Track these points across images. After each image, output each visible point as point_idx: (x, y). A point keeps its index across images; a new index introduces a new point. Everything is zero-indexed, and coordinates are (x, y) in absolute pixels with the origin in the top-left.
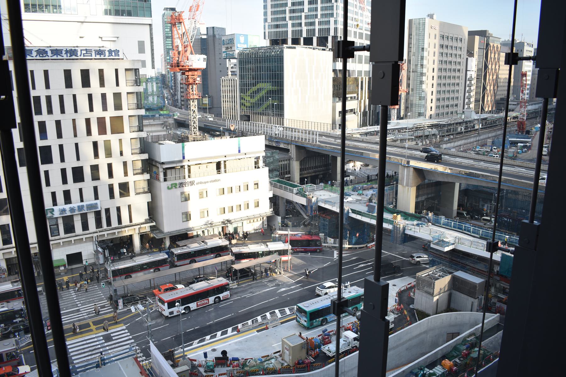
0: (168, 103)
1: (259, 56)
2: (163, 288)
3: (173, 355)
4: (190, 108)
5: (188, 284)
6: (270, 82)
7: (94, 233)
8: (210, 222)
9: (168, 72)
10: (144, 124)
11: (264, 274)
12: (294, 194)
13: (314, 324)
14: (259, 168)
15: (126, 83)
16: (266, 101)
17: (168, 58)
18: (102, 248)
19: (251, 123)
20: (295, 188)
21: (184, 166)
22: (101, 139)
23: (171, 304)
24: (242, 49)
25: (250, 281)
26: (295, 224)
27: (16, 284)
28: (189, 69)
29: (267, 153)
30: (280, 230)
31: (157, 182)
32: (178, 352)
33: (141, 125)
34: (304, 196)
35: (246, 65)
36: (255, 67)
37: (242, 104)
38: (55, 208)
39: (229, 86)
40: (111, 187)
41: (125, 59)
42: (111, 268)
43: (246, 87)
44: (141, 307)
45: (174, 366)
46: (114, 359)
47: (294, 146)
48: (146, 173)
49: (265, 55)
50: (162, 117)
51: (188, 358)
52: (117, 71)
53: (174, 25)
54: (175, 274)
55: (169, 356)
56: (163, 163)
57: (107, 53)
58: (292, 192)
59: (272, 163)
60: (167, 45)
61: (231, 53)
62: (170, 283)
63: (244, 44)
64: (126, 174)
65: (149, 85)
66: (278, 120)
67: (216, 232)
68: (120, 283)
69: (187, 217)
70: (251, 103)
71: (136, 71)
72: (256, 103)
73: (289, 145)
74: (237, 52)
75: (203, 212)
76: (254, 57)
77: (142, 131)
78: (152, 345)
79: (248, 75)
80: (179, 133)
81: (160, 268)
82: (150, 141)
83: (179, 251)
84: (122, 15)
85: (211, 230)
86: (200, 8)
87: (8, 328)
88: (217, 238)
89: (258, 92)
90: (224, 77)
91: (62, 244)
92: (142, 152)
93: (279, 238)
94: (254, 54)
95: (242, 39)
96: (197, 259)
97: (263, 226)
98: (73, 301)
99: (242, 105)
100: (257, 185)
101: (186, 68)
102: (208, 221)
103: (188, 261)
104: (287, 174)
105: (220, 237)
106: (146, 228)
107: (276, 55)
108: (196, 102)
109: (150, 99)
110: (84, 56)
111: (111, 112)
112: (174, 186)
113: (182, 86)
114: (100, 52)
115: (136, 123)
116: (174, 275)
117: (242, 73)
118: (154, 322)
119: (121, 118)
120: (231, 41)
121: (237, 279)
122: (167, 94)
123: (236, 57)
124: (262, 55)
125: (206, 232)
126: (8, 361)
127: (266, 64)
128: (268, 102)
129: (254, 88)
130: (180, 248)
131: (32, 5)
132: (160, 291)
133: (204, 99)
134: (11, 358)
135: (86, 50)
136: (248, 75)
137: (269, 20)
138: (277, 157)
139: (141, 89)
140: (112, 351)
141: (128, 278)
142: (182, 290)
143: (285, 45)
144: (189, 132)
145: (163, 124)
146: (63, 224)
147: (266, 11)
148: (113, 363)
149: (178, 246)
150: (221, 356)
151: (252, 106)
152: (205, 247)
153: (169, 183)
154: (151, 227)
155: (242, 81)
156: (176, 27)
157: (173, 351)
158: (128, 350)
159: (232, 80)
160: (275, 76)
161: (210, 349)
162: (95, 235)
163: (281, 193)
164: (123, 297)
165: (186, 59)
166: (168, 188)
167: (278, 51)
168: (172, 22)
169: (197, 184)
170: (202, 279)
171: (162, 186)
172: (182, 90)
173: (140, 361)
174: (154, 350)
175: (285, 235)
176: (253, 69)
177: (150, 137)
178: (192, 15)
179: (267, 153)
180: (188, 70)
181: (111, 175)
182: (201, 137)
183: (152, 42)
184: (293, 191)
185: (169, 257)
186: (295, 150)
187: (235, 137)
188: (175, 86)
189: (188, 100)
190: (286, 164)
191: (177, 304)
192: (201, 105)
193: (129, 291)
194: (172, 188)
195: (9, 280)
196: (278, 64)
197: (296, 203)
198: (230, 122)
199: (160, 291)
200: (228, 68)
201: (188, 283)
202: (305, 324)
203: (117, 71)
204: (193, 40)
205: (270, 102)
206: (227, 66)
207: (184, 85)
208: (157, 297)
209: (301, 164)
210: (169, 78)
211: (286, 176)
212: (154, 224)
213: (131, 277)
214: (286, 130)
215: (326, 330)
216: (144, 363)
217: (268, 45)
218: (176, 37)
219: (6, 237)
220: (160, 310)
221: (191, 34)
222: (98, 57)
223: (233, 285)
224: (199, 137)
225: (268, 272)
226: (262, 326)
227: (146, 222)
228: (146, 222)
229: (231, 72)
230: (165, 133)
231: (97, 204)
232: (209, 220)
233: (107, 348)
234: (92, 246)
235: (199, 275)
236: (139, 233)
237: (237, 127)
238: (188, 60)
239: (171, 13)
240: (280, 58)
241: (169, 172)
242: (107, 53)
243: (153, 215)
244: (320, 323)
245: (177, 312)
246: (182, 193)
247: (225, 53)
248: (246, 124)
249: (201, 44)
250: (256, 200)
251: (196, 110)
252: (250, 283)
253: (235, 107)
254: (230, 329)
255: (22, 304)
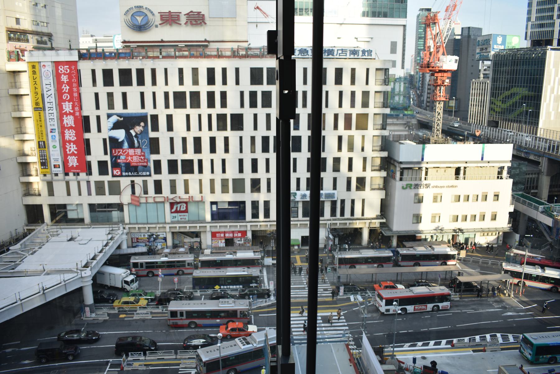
0: (414, 104)
1: (517, 58)
2: (384, 284)
3: (383, 352)
4: (435, 109)
5: (409, 285)
6: (527, 87)
7: (328, 220)
8: (440, 228)
9: (417, 73)
10: (387, 123)
11: (491, 292)
12: (539, 213)
13: (541, 360)
14: (503, 179)
15: (376, 82)
16: (519, 107)
17: (419, 58)
18: (333, 235)
19: (499, 130)
20: (541, 206)
21: (422, 168)
22: (346, 134)
23: (389, 302)
24: (498, 50)
25: (474, 297)
26: (535, 245)
27: (257, 254)
28: (439, 70)
29: (514, 164)
30: (516, 248)
31: (393, 181)
32: (388, 350)
33: (385, 123)
34: (551, 216)
35: (501, 68)
36: (511, 70)
37: (491, 109)
38: (298, 192)
39: (480, 89)
40: (349, 180)
41: (377, 59)
42: (339, 255)
43: (499, 90)
44: (360, 298)
45: (382, 362)
46: (327, 340)
47: (547, 159)
48: (383, 170)
49: (524, 57)
50: (405, 117)
51: (397, 359)
52: (368, 70)
53: (427, 25)
54: (397, 273)
55: (379, 352)
56: (401, 163)
57: (361, 53)
58: (537, 209)
59: (518, 174)
60: (419, 45)
61: (485, 54)
62: (391, 281)
63: (501, 45)
64: (364, 169)
65: (397, 85)
66: (530, 129)
67: (445, 239)
68: (345, 272)
69: (417, 220)
70: (502, 108)
71: (386, 70)
72: (507, 109)
73: (541, 158)
74: (492, 53)
75: (435, 217)
76: (511, 58)
77: (385, 129)
78: (364, 337)
79: (502, 78)
80: (420, 134)
81: (384, 265)
82: (391, 139)
83: (405, 252)
84: (378, 17)
85: (440, 236)
86: (457, 7)
87: (245, 290)
88: (446, 246)
89: (511, 97)
90: (475, 80)
91: (299, 225)
92: (382, 149)
93: (514, 258)
94: (511, 56)
95: (499, 40)
96: (421, 263)
97: (498, 241)
98: (300, 279)
99: (492, 110)
100: (497, 197)
101: (436, 69)
102: (439, 227)
103: (412, 263)
104: (533, 189)
105: (449, 245)
106: (376, 224)
107: (537, 58)
108: (442, 105)
109: (397, 98)
110: (340, 55)
111: (358, 109)
112: (409, 186)
113: (429, 87)
114: (354, 52)
115: (380, 121)
116: (396, 274)
117: (495, 75)
118: (369, 315)
119: (366, 115)
120: (487, 42)
121: (460, 291)
122: (413, 95)
123: (491, 59)
124: (521, 57)
125: (435, 238)
126: (240, 318)
127: (527, 67)
128: (522, 109)
129: (507, 93)
130: (406, 249)
131: (300, 9)
132: (380, 286)
133: (451, 102)
134: (244, 316)
135: (342, 50)
136: (502, 78)
137: (533, 19)
138: (524, 169)
139: (388, 88)
140: (327, 332)
141: (352, 268)
142: (401, 291)
143: (549, 47)
144: (431, 134)
145: (405, 124)
146: (303, 208)
147: (530, 9)
148: (326, 344)
149: (404, 246)
150: (430, 366)
151: (503, 112)
152: (432, 252)
153: (404, 183)
154: (381, 223)
155: (494, 85)
156: (430, 27)
157: (383, 348)
158: (341, 336)
159: (483, 83)
160: (533, 80)
161: (420, 356)
162: (329, 222)
163: (523, 208)
164: (345, 285)
165: (437, 60)
166: (403, 188)
167: (540, 53)
168: (426, 22)
169: (433, 187)
170: (424, 284)
171: (398, 185)
172: (429, 91)
173: (351, 349)
174: (365, 341)
175: (521, 255)
176: (508, 72)
177: (391, 136)
178: (448, 15)
179: (514, 164)
180: (438, 71)
181: (350, 168)
182: (443, 140)
183: (404, 43)
184: (538, 209)
185: (394, 255)
186: (546, 163)
187: (479, 143)
188: (422, 87)
189: (434, 102)
190: (534, 178)
191: (394, 303)
192: (447, 107)
193: (351, 281)
194: (406, 188)
195: (252, 249)
196: (538, 67)
197: (540, 222)
198: (475, 127)
199: (380, 286)
200: (480, 70)
201: (409, 285)
202: (529, 357)
203: (368, 70)
204: (446, 41)
205: (523, 108)
206: (480, 68)
207: (432, 86)
208: (376, 292)
209: (552, 180)
210: (417, 78)
211: (532, 191)
212: (384, 221)
213: (355, 267)
214: (539, 141)
215: (554, 370)
216: (354, 351)
217: (529, 46)
218: (429, 38)
219: (255, 212)
220: (377, 305)
221: (445, 35)
222: (352, 56)
223: (455, 297)
224: (441, 140)
225: (495, 291)
226: (479, 347)
227: (377, 218)
228: (377, 218)
229: (484, 74)
230: (406, 133)
231: (334, 194)
232: (440, 225)
233: (324, 329)
234: (324, 232)
235: (421, 279)
236: (369, 228)
237: (483, 133)
238: (439, 61)
239: (426, 13)
240: (542, 61)
241: (405, 172)
242: (361, 53)
243: (384, 212)
244: (547, 360)
245: (393, 311)
246: (416, 195)
247: (479, 55)
248: (493, 131)
249: (454, 45)
250: (483, 213)
251: (441, 112)
252: (473, 299)
253: (483, 111)
254: (444, 341)
255: (259, 271)
